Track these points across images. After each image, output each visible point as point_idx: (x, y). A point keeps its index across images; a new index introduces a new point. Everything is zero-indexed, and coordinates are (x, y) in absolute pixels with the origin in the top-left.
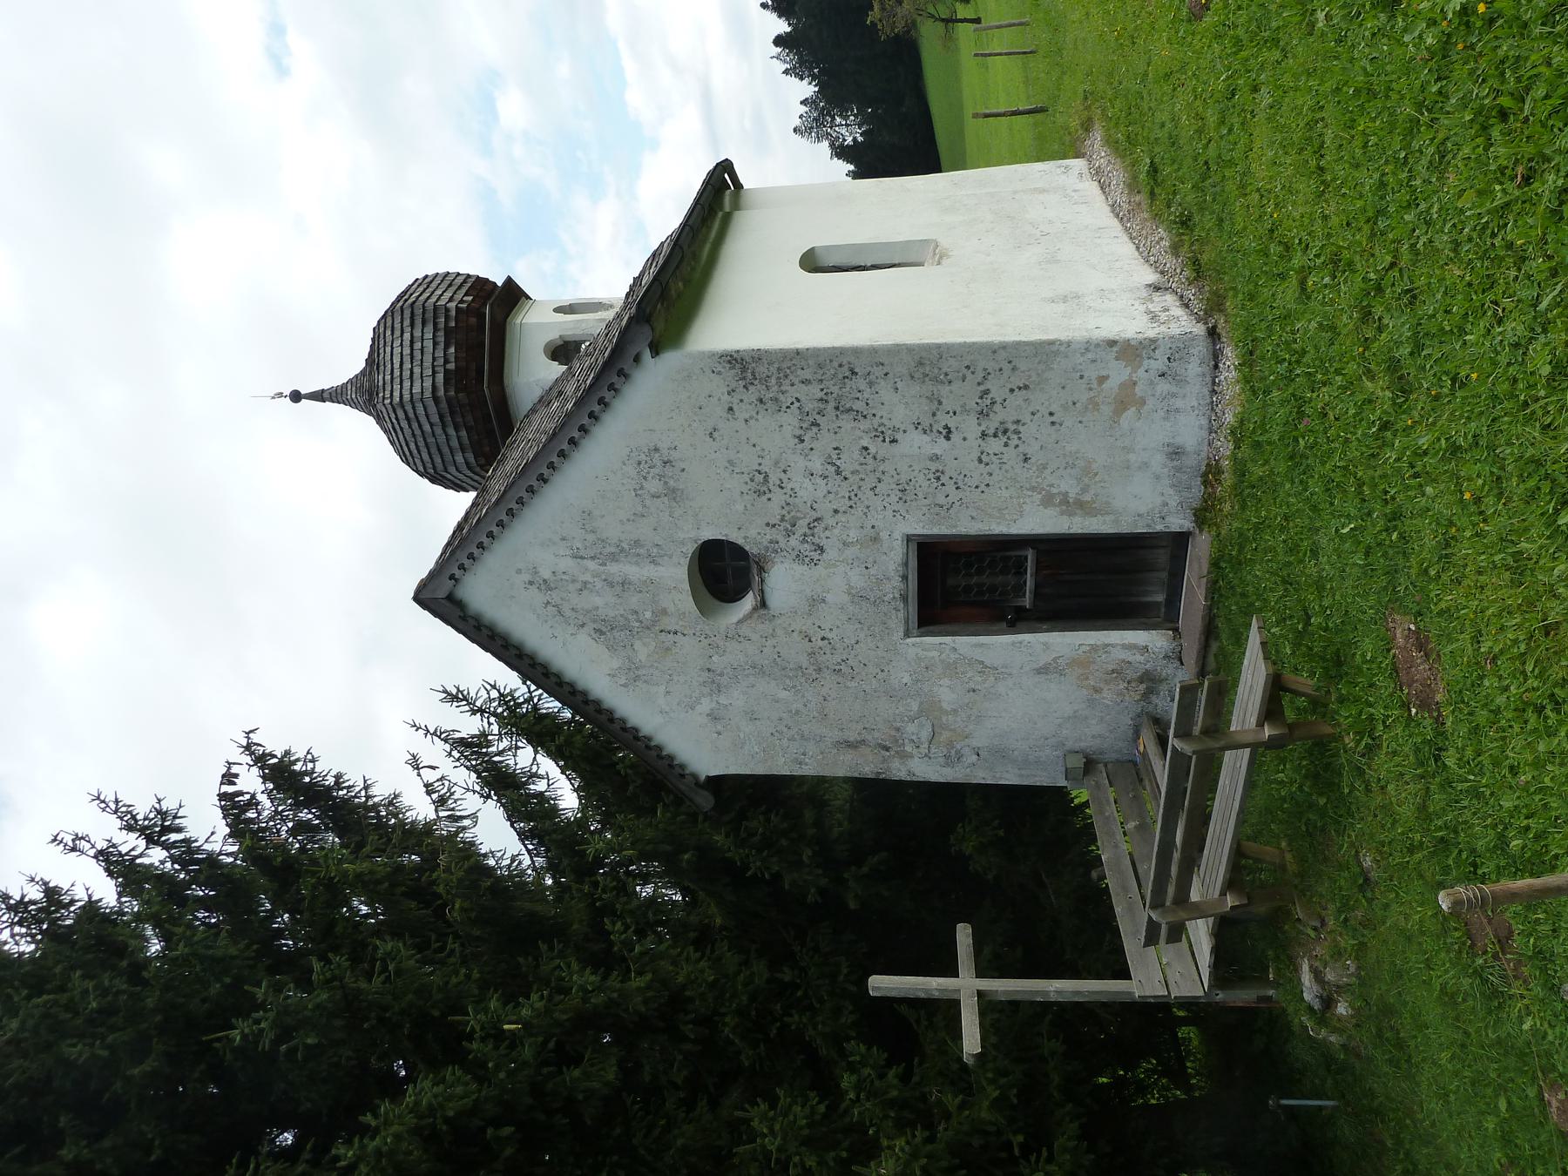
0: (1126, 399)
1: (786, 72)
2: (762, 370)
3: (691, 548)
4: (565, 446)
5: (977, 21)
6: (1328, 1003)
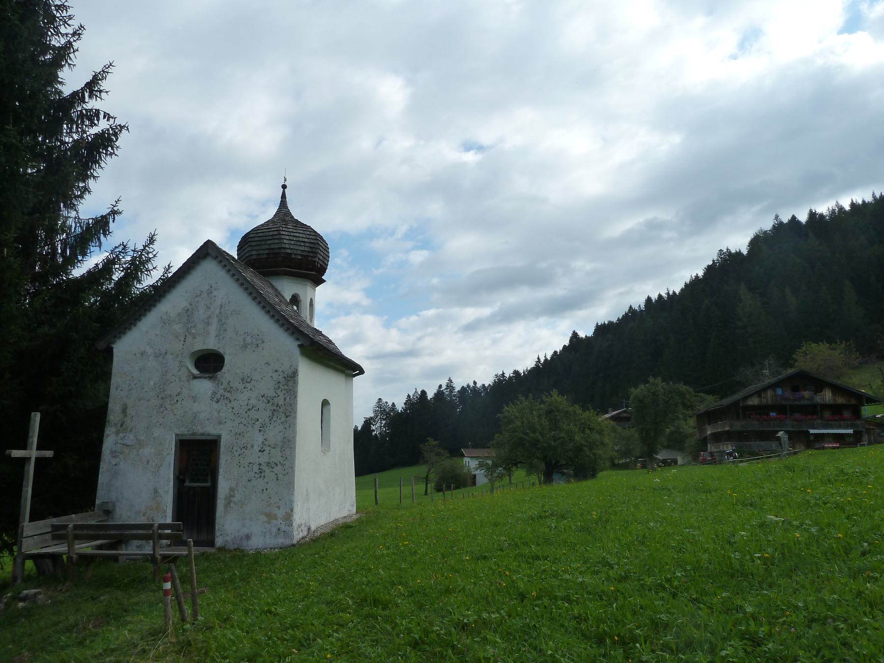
0: (270, 516)
1: (409, 396)
2: (290, 383)
3: (221, 351)
4: (267, 309)
5: (426, 494)
6: (24, 599)
